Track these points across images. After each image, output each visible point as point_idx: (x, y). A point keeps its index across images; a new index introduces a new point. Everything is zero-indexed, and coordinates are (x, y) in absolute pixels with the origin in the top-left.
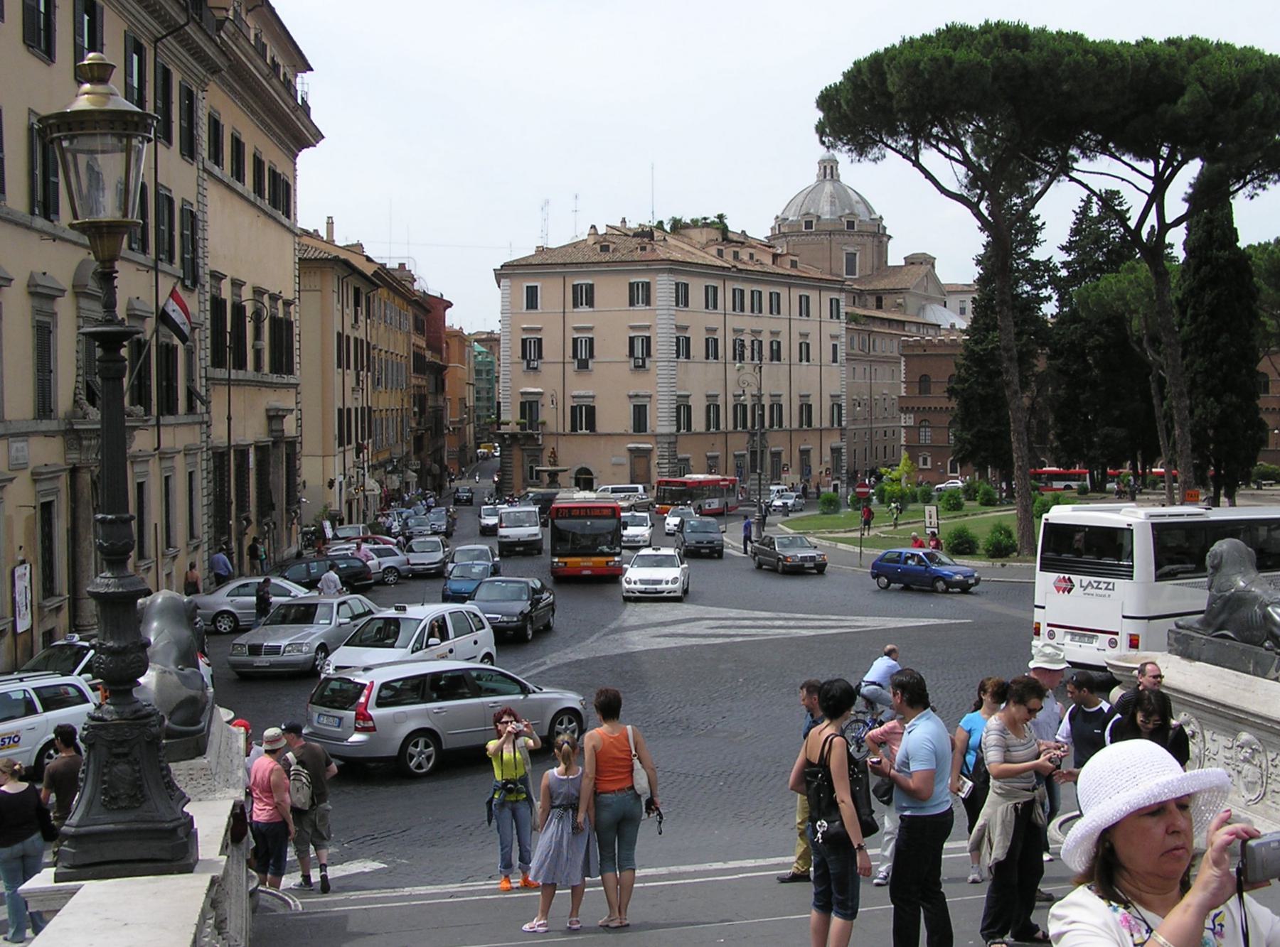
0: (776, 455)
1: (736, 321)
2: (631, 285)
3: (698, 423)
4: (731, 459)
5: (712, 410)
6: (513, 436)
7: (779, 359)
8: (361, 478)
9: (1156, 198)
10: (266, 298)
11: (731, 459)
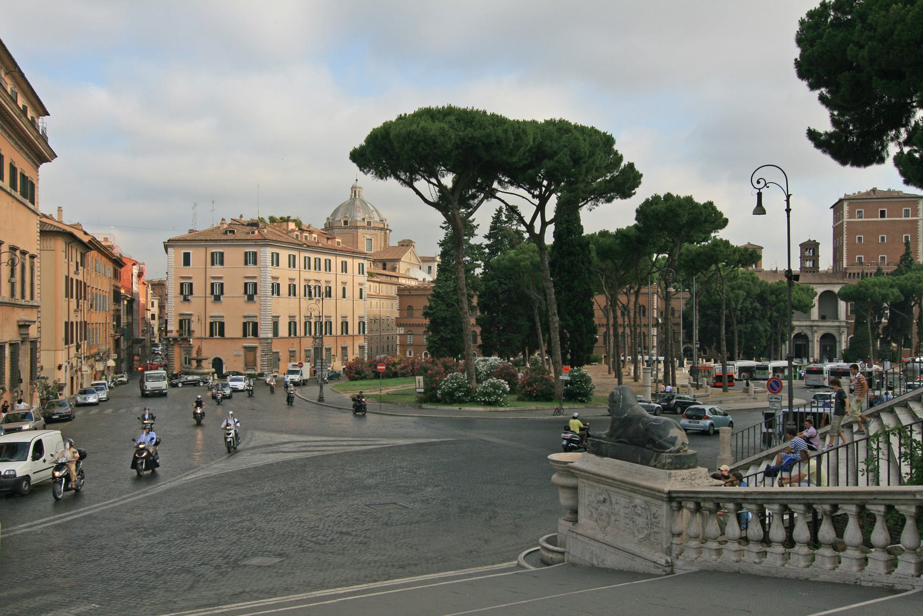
0: (329, 350)
1: (307, 274)
2: (246, 253)
3: (283, 331)
4: (303, 352)
5: (292, 325)
6: (175, 339)
7: (330, 296)
8: (79, 364)
9: (541, 208)
10: (18, 253)
11: (303, 352)
